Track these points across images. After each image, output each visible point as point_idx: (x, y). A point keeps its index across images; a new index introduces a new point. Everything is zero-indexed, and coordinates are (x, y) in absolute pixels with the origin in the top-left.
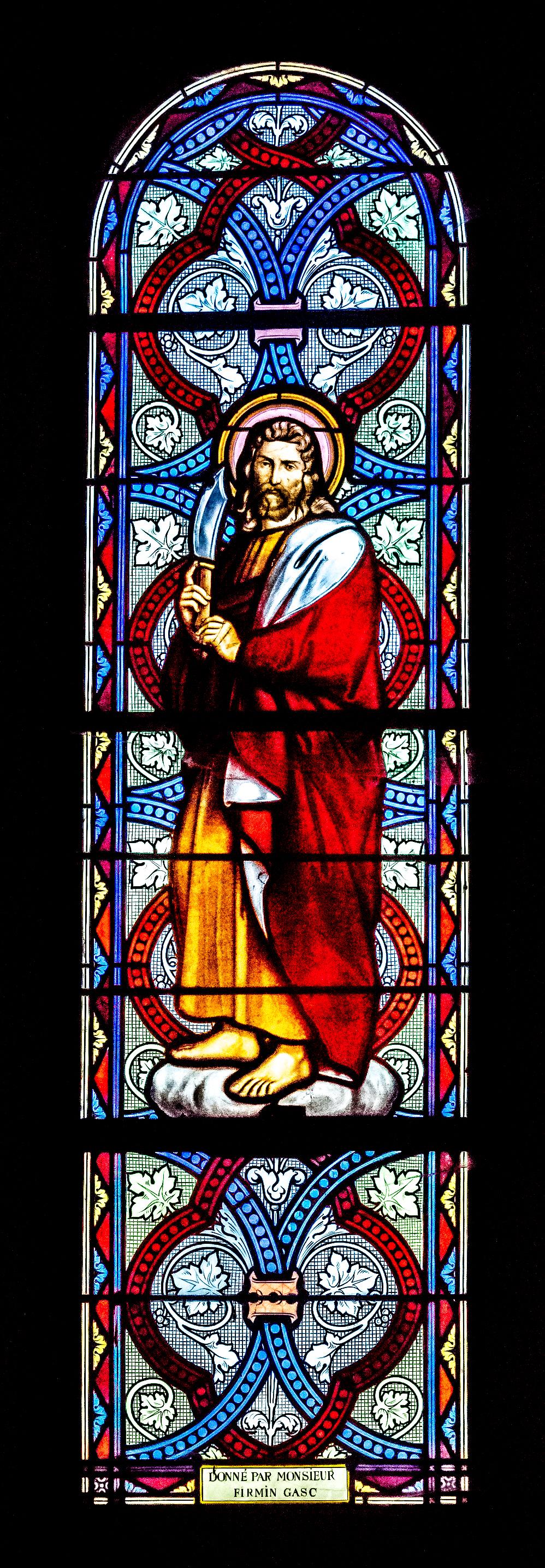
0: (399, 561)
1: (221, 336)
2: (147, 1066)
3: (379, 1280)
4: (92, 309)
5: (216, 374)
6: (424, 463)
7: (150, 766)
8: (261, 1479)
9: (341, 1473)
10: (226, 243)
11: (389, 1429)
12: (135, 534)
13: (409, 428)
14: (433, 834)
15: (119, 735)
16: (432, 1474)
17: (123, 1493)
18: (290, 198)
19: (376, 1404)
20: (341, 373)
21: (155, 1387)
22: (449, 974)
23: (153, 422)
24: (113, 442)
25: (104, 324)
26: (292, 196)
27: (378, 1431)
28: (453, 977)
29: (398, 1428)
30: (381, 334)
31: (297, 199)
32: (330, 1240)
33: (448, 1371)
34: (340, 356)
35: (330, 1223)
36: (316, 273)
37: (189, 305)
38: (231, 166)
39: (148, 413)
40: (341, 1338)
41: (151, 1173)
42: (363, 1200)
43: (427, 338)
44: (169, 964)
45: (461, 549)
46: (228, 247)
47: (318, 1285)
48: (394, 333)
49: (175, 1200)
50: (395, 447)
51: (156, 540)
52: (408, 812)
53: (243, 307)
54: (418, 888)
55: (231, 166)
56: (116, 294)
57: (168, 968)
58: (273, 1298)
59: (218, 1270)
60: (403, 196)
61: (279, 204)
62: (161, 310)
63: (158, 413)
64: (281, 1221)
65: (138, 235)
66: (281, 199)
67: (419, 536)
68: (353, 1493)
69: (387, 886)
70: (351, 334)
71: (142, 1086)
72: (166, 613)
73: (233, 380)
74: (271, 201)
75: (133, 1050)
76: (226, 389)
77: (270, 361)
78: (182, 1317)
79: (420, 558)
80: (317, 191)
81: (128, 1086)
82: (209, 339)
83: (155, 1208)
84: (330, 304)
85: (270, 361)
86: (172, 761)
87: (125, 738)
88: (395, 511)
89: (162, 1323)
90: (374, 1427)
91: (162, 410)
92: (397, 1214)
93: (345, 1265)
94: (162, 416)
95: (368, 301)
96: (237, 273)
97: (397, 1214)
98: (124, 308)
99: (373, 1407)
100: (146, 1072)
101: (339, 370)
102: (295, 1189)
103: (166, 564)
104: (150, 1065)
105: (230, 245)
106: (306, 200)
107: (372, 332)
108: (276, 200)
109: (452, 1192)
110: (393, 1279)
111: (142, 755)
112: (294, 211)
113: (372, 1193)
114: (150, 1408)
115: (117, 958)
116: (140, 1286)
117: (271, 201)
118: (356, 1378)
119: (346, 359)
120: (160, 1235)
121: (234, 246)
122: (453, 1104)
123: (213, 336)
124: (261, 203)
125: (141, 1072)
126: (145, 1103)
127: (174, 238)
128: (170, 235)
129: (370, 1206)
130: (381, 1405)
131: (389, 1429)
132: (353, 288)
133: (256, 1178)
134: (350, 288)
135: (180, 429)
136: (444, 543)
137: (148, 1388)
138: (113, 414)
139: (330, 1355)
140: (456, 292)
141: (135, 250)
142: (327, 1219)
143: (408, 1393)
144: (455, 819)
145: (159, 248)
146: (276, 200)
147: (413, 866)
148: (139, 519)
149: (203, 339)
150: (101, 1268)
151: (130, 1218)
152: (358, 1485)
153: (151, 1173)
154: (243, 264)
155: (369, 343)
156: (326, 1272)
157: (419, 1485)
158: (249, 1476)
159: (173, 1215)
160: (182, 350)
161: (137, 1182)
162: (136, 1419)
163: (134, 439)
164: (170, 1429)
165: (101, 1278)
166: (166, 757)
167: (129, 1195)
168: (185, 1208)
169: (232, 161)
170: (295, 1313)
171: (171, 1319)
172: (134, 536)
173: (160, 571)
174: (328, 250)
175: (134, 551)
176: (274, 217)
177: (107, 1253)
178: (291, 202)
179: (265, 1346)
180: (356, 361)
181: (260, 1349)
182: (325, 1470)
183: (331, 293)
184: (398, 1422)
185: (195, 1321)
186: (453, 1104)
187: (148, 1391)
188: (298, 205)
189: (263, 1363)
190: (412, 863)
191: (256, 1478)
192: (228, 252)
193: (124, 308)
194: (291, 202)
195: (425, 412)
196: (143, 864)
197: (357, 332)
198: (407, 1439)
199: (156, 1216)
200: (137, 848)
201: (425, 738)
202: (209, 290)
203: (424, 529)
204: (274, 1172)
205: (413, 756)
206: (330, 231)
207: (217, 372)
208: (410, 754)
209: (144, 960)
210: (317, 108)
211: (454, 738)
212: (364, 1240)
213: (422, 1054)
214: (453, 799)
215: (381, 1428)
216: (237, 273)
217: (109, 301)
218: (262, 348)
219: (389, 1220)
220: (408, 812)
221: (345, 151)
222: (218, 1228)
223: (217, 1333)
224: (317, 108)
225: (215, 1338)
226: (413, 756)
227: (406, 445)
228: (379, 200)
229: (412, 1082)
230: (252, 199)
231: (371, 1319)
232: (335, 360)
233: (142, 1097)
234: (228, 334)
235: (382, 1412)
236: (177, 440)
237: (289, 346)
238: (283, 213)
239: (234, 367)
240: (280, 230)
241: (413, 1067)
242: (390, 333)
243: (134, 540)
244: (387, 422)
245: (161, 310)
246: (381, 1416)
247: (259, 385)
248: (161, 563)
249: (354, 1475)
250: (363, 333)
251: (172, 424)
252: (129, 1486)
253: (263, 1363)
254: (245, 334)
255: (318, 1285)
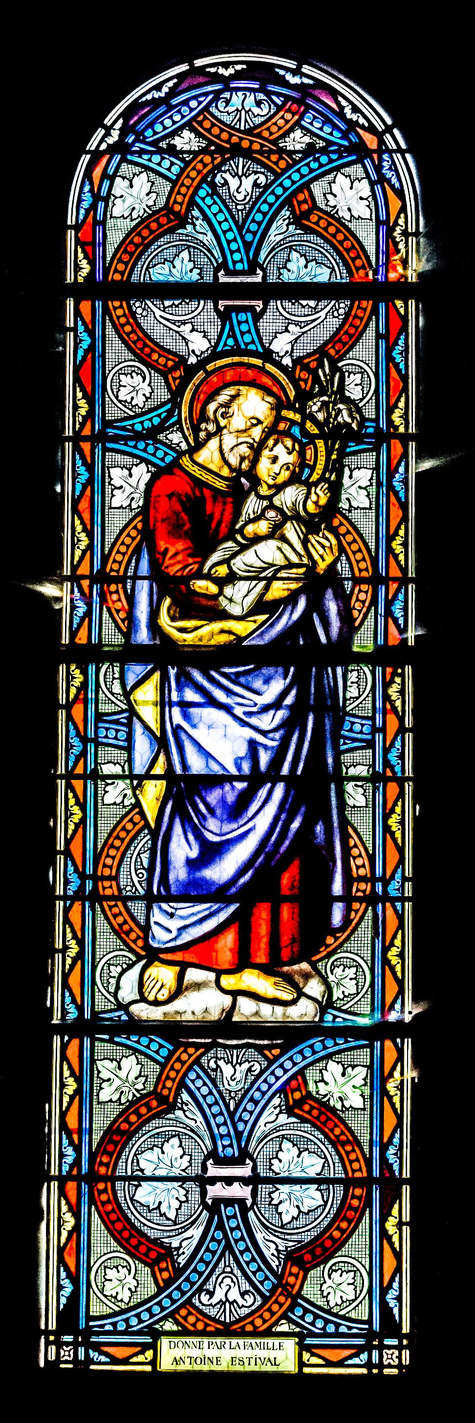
0: (351, 506)
1: (188, 304)
2: (115, 971)
3: (326, 1165)
4: (70, 278)
5: (184, 338)
6: (374, 417)
7: (126, 401)
8: (216, 1347)
9: (290, 1345)
10: (183, 1103)
11: (337, 1305)
12: (99, 1072)
13: (360, 384)
14: (381, 615)
15: (91, 669)
16: (375, 1347)
17: (89, 1361)
18: (245, 1062)
19: (325, 1282)
20: (296, 339)
21: (124, 959)
22: (392, 1164)
23: (111, 1274)
24: (74, 1215)
25: (81, 292)
26: (247, 1061)
27: (326, 1307)
28: (398, 769)
29: (345, 1304)
30: (334, 305)
31: (252, 1063)
32: (281, 1128)
33: (391, 1244)
34: (297, 324)
35: (281, 1112)
36: (266, 1136)
37: (160, 274)
38: (199, 146)
39: (120, 372)
40: (301, 328)
41: (122, 764)
42: (321, 203)
43: (375, 311)
44: (137, 875)
45: (408, 378)
46: (185, 1108)
47: (270, 1169)
48: (346, 305)
49: (151, 203)
50: (341, 996)
51: (117, 1076)
52: (354, 740)
53: (209, 278)
54: (370, 508)
55: (199, 146)
56: (92, 263)
57: (135, 879)
58: (229, 1181)
59: (191, 265)
60: (350, 766)
61: (234, 1067)
62: (134, 278)
63: (130, 372)
64: (245, 220)
65: (112, 207)
66: (237, 1063)
67: (369, 484)
68: (301, 1364)
69: (343, 217)
70: (307, 305)
71: (112, 990)
72: (132, 848)
73: (199, 344)
74: (227, 1064)
75: (104, 956)
76: (193, 351)
77: (232, 328)
78: (159, 308)
79: (367, 801)
80: (271, 1057)
81: (98, 988)
82: (177, 306)
83: (134, 209)
84: (287, 277)
85: (232, 328)
86: (132, 1292)
87: (98, 670)
88: (343, 1057)
89: (141, 314)
90: (322, 1303)
91: (133, 369)
92: (352, 215)
93: (302, 261)
94: (134, 374)
95: (323, 275)
96: (192, 1130)
97: (352, 215)
98: (99, 276)
99: (322, 1285)
100: (114, 977)
101: (296, 336)
102: (251, 1078)
103: (139, 506)
104: (119, 969)
105: (187, 1105)
106: (260, 1065)
107: (326, 304)
108: (232, 1063)
109: (398, 948)
110: (340, 1164)
111: (104, 1286)
112: (249, 1074)
113: (329, 197)
114: (128, 387)
115: (89, 870)
116: (122, 273)
117: (227, 1064)
118: (308, 1257)
119: (301, 328)
120: (133, 829)
121: (190, 1106)
122: (398, 749)
123: (180, 304)
124: (218, 1066)
125: (111, 977)
126: (115, 1005)
127: (134, 1095)
128: (131, 1094)
129: (329, 209)
130: (329, 1282)
131: (337, 1305)
132: (300, 1153)
133: (222, 181)
134: (297, 1152)
135: (151, 387)
136: (385, 1248)
137: (126, 368)
138: (80, 919)
139: (291, 342)
140: (405, 417)
141: (110, 223)
142: (279, 1108)
143: (355, 1271)
144: (400, 761)
145: (131, 510)
146: (232, 1063)
147: (362, 786)
148: (115, 467)
149: (171, 306)
150: (70, 1151)
151: (111, 217)
152: (306, 1356)
153: (122, 764)
154: (198, 1123)
155: (323, 314)
156: (277, 1157)
157: (364, 1356)
158: (206, 1345)
159: (150, 216)
160: (152, 316)
161: (105, 1068)
162: (108, 689)
163: (108, 394)
164: (132, 1300)
165: (69, 1160)
166: (126, 1288)
167: (96, 1081)
168: (161, 209)
169: (199, 142)
170: (249, 1197)
171: (149, 310)
172: (98, 1074)
173: (135, 223)
174: (277, 1115)
175: (110, 495)
176: (229, 1079)
177: (89, 389)
178: (246, 1066)
179: (221, 1227)
180: (310, 330)
181: (229, 336)
182: (276, 1341)
183: (279, 1156)
184: (344, 1299)
185: (171, 312)
186: (398, 749)
187: (126, 372)
188: (253, 1069)
189: (219, 1242)
190: (360, 783)
191: (211, 1347)
192: (184, 1111)
193: (99, 276)
194: (246, 1066)
195: (369, 965)
196: (113, 783)
197: (312, 303)
198: (353, 1315)
199: (135, 215)
200: (108, 769)
201: (373, 673)
202: (177, 262)
203: (374, 478)
204: (229, 1302)
205: (358, 1292)
206: (280, 1097)
207: (185, 336)
208: (355, 1290)
209: (114, 873)
210: (279, 95)
211: (398, 1296)
212: (322, 241)
213: (367, 1267)
214: (398, 876)
215: (328, 1304)
216: (192, 1130)
217: (86, 268)
218: (224, 316)
219: (344, 221)
220: (354, 740)
221: (305, 135)
222: (189, 228)
223: (191, 323)
224: (279, 95)
225: (189, 327)
226: (358, 1292)
227: (353, 698)
228: (334, 182)
229: (365, 392)
230: (209, 1061)
231: (329, 312)
232: (291, 328)
233: (112, 999)
234: (194, 304)
235: (330, 1290)
236: (148, 395)
237: (249, 314)
238: (238, 1076)
239: (200, 332)
240: (235, 1092)
241: (361, 973)
242: (342, 305)
243: (98, 1077)
244: (334, 973)
245: (134, 278)
246: (329, 1293)
247: (223, 347)
248: (134, 505)
249: (302, 1347)
250: (317, 305)
251: (129, 1274)
252: (93, 1354)
253: (219, 1242)
254: (210, 305)
255: (270, 1169)
